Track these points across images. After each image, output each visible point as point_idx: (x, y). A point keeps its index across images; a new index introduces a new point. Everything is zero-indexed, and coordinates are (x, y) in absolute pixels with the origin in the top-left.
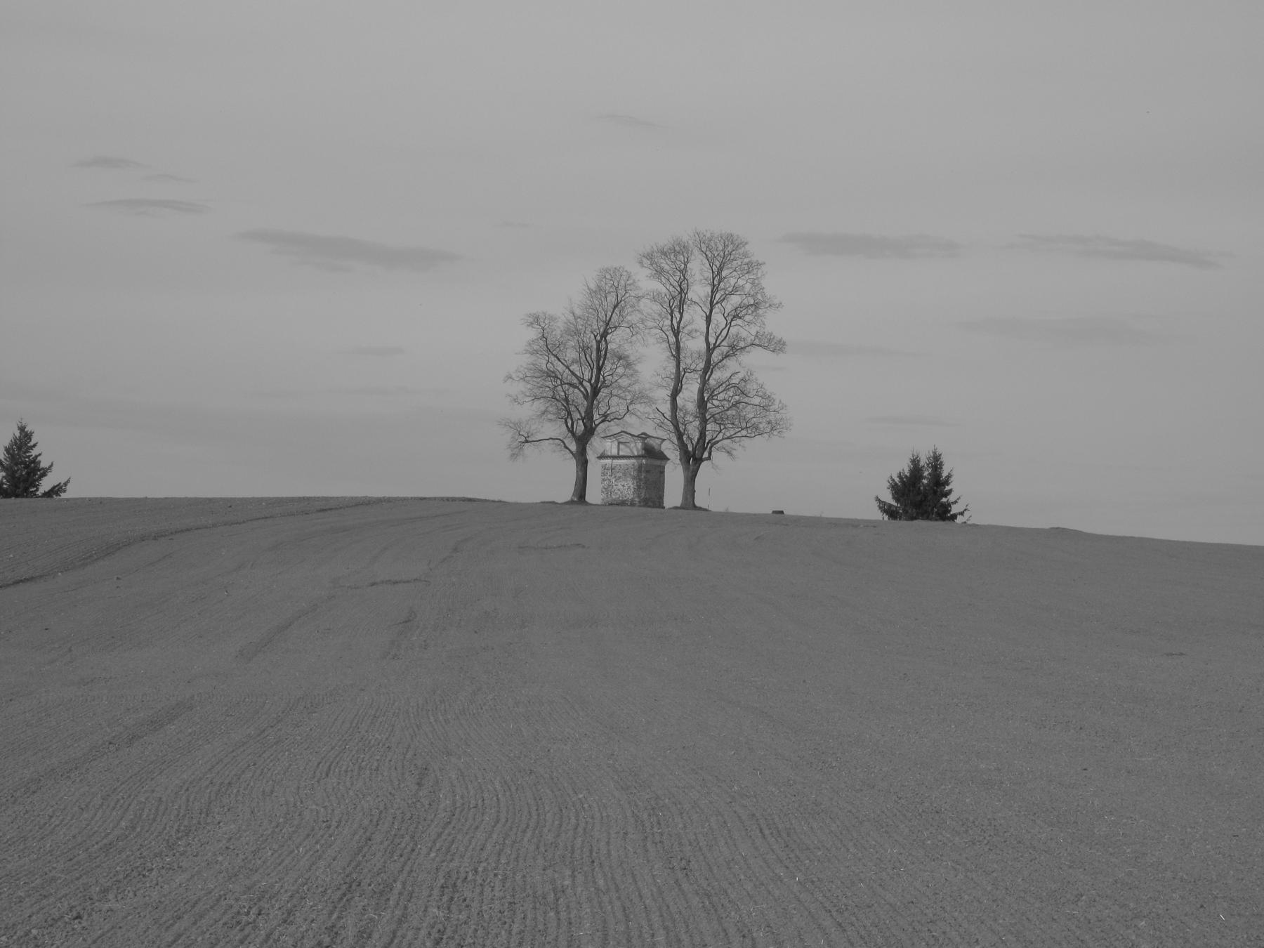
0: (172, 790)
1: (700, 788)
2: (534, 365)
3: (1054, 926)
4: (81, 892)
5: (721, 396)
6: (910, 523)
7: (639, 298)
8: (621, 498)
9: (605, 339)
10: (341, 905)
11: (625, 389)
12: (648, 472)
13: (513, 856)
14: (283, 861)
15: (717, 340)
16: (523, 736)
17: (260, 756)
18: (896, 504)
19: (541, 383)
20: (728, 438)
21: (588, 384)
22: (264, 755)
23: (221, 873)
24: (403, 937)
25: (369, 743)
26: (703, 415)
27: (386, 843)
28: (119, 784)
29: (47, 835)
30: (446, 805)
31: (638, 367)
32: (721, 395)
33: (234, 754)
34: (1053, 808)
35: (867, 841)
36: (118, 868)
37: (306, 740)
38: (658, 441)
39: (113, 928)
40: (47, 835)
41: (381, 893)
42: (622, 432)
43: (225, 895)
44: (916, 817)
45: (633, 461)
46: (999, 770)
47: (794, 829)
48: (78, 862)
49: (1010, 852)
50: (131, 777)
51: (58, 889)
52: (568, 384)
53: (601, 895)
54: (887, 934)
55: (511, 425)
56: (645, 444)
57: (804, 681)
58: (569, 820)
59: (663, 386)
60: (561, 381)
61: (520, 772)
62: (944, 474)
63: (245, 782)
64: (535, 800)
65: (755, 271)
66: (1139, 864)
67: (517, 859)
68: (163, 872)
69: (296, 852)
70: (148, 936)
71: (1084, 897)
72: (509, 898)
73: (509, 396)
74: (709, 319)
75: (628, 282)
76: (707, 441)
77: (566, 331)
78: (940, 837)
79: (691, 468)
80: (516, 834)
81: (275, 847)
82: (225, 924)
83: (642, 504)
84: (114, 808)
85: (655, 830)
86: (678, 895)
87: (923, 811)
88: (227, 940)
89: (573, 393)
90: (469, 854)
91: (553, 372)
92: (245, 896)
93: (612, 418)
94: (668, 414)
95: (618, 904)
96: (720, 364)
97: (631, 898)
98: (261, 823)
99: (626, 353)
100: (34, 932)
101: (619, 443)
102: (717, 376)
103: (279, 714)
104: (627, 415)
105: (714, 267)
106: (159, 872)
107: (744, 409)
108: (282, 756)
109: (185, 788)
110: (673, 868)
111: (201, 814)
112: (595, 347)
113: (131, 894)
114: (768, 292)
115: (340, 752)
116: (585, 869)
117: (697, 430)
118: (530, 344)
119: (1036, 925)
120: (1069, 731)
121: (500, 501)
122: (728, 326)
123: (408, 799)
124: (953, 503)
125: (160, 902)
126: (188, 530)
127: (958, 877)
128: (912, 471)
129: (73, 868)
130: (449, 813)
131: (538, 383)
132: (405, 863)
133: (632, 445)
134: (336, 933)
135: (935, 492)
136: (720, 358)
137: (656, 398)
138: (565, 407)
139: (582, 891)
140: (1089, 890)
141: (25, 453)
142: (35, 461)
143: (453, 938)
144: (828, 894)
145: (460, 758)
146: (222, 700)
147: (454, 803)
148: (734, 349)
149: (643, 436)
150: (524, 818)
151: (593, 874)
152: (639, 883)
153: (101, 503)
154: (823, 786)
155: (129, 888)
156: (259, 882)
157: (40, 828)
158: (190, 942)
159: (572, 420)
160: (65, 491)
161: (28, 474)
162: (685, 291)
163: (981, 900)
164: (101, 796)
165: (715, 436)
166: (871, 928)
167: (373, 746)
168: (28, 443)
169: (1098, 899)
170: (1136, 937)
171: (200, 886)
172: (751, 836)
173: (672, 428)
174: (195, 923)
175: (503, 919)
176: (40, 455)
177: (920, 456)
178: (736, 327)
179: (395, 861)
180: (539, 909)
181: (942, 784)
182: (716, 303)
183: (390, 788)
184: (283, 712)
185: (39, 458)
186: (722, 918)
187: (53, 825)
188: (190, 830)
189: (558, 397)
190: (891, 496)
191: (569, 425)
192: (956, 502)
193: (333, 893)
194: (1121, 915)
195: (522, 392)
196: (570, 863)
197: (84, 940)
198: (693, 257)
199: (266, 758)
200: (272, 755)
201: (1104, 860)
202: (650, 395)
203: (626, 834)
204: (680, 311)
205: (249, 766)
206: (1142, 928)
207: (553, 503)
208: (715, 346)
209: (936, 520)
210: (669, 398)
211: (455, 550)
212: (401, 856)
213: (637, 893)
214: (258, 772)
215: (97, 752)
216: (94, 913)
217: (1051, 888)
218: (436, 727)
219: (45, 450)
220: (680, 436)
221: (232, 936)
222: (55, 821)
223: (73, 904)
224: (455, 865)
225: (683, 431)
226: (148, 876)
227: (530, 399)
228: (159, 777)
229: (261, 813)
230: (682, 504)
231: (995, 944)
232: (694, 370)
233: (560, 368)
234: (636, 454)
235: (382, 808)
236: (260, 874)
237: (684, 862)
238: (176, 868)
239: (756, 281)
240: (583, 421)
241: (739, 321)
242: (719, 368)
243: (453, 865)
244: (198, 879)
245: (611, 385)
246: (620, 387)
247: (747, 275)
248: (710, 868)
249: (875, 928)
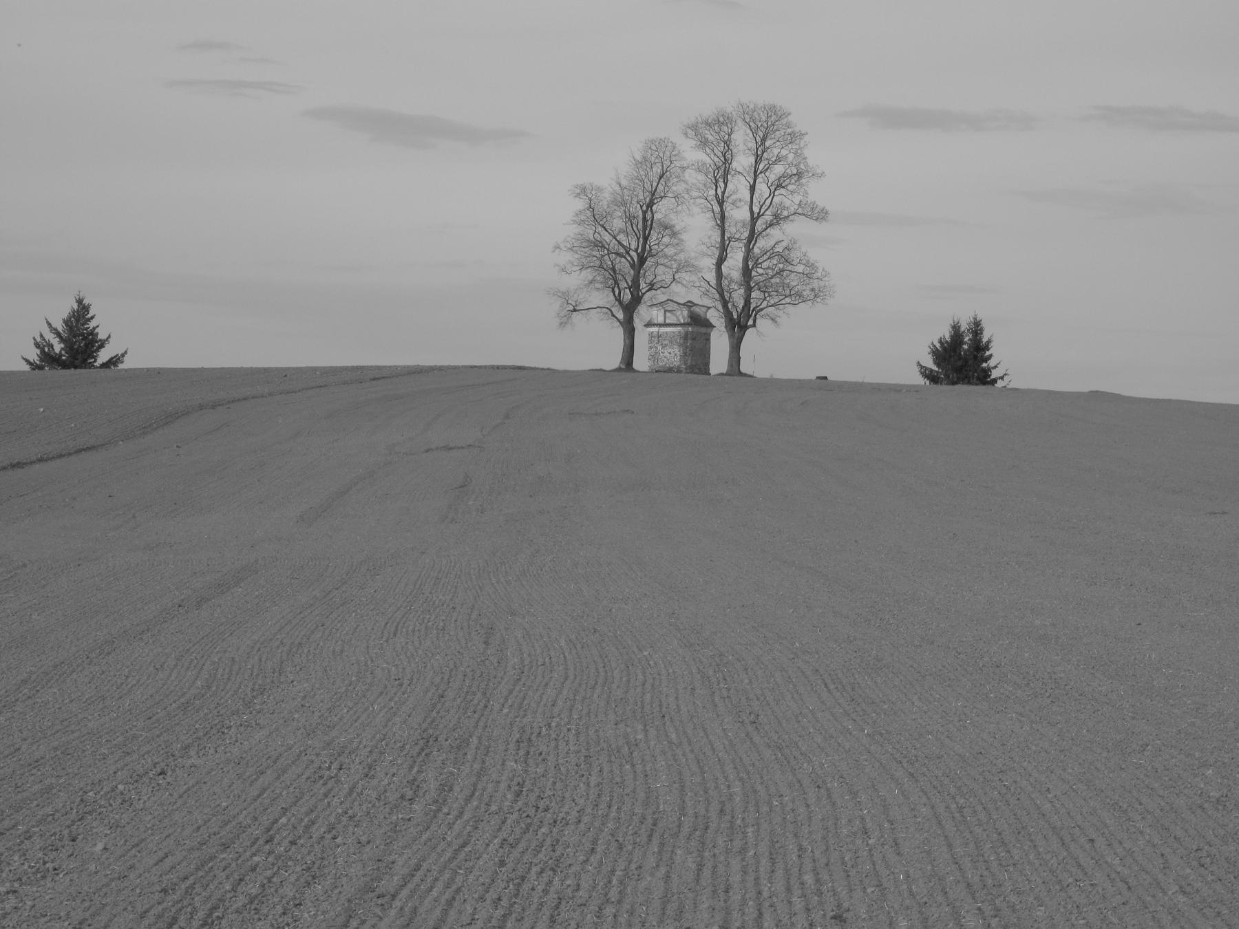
0: (244, 651)
1: (762, 645)
2: (582, 235)
3: (1124, 775)
4: (163, 749)
5: (765, 265)
6: (950, 387)
7: (684, 169)
9: (651, 209)
10: (421, 759)
11: (671, 258)
12: (694, 339)
13: (584, 712)
14: (358, 718)
15: (760, 209)
16: (584, 596)
17: (327, 617)
18: (937, 369)
19: (588, 253)
20: (772, 306)
21: (635, 254)
22: (331, 616)
23: (298, 730)
24: (484, 789)
25: (434, 604)
26: (748, 283)
27: (459, 700)
28: (191, 645)
29: (126, 694)
30: (514, 663)
31: (684, 237)
32: (765, 263)
33: (302, 615)
34: (1110, 661)
35: (931, 695)
36: (197, 726)
37: (371, 601)
38: (704, 309)
39: (197, 783)
40: (126, 694)
41: (459, 747)
42: (668, 300)
43: (305, 751)
44: (977, 671)
45: (679, 328)
46: (1054, 625)
47: (858, 683)
48: (158, 720)
49: (1073, 704)
50: (203, 638)
51: (140, 746)
52: (614, 253)
53: (675, 748)
54: (959, 784)
55: (559, 294)
56: (691, 311)
57: (856, 541)
58: (637, 676)
59: (708, 255)
60: (608, 250)
61: (584, 631)
62: (985, 340)
63: (315, 642)
64: (602, 657)
65: (798, 142)
66: (1201, 715)
67: (588, 714)
68: (242, 729)
69: (371, 709)
70: (233, 790)
71: (1149, 747)
72: (584, 752)
73: (557, 265)
74: (752, 189)
75: (674, 153)
76: (751, 309)
77: (613, 201)
78: (1002, 691)
79: (736, 335)
80: (585, 690)
81: (350, 704)
82: (308, 778)
83: (688, 371)
84: (188, 668)
85: (722, 685)
86: (750, 748)
87: (984, 666)
88: (311, 794)
89: (620, 262)
90: (540, 710)
91: (600, 242)
92: (326, 752)
93: (659, 286)
94: (713, 282)
95: (691, 756)
96: (764, 233)
97: (703, 751)
98: (334, 681)
99: (671, 223)
100: (121, 787)
101: (665, 311)
102: (761, 244)
103: (344, 577)
104: (673, 284)
105: (758, 137)
106: (238, 729)
107: (787, 276)
108: (349, 617)
109: (256, 648)
110: (743, 722)
111: (273, 673)
112: (641, 216)
113: (212, 751)
114: (811, 162)
115: (406, 613)
116: (656, 723)
117: (742, 298)
118: (577, 215)
119: (1104, 774)
120: (1120, 587)
121: (548, 369)
122: (772, 195)
123: (477, 657)
125: (241, 757)
126: (245, 399)
127: (1024, 729)
128: (952, 337)
129: (153, 726)
130: (519, 671)
131: (586, 253)
132: (479, 719)
133: (679, 313)
134: (418, 786)
135: (975, 357)
136: (764, 227)
137: (701, 267)
138: (612, 276)
139: (655, 744)
140: (1153, 740)
141: (83, 325)
142: (92, 333)
143: (532, 790)
144: (897, 746)
145: (524, 617)
146: (286, 563)
147: (522, 660)
148: (777, 219)
149: (689, 304)
150: (592, 675)
151: (665, 728)
152: (711, 737)
153: (159, 373)
154: (883, 642)
155: (210, 745)
156: (337, 737)
157: (117, 688)
158: (275, 796)
159: (619, 289)
160: (122, 362)
161: (86, 345)
162: (729, 162)
163: (1048, 751)
164: (175, 657)
165: (759, 304)
166: (943, 779)
167: (438, 607)
168: (86, 315)
169: (1163, 748)
170: (1205, 785)
171: (279, 743)
172: (816, 691)
173: (717, 296)
174: (278, 778)
175: (579, 772)
176: (98, 326)
177: (960, 322)
178: (781, 196)
179: (469, 717)
180: (614, 762)
181: (999, 640)
182: (761, 173)
183: (458, 648)
184: (347, 575)
185: (96, 331)
186: (795, 770)
187: (130, 685)
188: (264, 689)
189: (605, 267)
190: (932, 361)
191: (617, 293)
192: (996, 367)
193: (411, 748)
194: (1188, 763)
195: (569, 261)
196: (641, 718)
197: (170, 795)
198: (737, 128)
199: (334, 618)
200: (339, 616)
201: (1166, 712)
202: (696, 263)
203: (693, 689)
204: (724, 182)
205: (317, 626)
206: (1209, 776)
207: (601, 370)
208: (759, 216)
209: (976, 384)
210: (714, 267)
211: (507, 417)
212: (475, 712)
213: (710, 747)
214: (327, 632)
215: (167, 614)
216: (177, 769)
217: (1116, 738)
218: (498, 588)
219: (102, 322)
220: (725, 304)
221: (316, 790)
222: (131, 681)
223: (156, 761)
224: (528, 720)
225: (728, 299)
226: (227, 733)
227: (578, 268)
228: (229, 638)
229: (333, 671)
230: (727, 371)
231: (1066, 793)
232: (738, 239)
233: (607, 238)
234: (682, 321)
235: (452, 666)
236: (338, 730)
237: (752, 716)
238: (254, 724)
239: (799, 151)
240: (630, 290)
241: (782, 191)
242: (763, 237)
243: (525, 721)
244: (277, 736)
245: (657, 254)
246: (666, 256)
247: (790, 145)
248: (779, 722)
249: (946, 778)
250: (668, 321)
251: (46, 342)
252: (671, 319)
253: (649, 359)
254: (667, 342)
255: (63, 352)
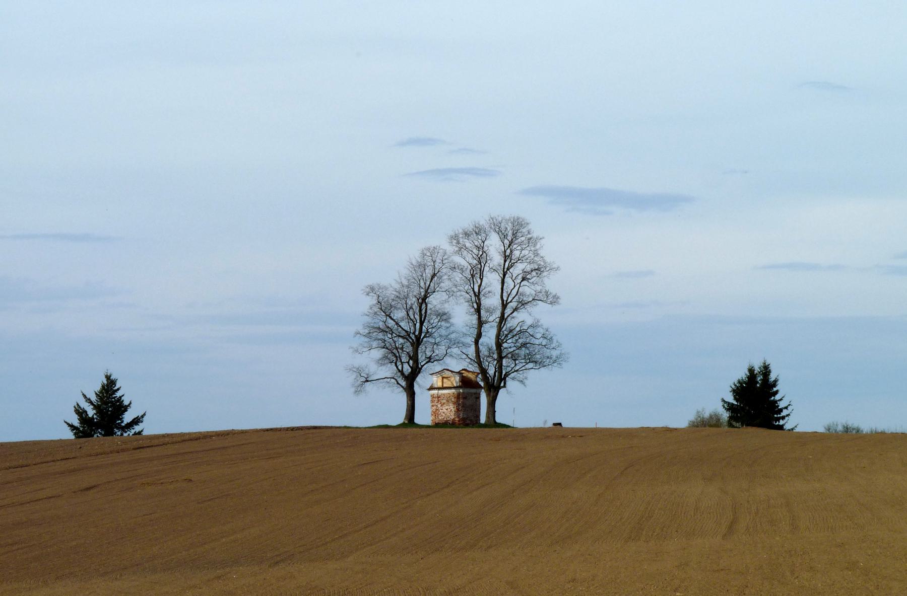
8: (445, 419)
12: (465, 398)
18: (736, 403)
45: (453, 391)
56: (463, 377)
76: (504, 374)
101: (443, 378)
124: (779, 400)
142: (120, 400)
160: (142, 422)
168: (114, 387)
176: (123, 396)
185: (123, 398)
190: (733, 398)
191: (400, 368)
192: (781, 400)
204: (480, 278)
219: (126, 392)
230: (486, 421)
234: (455, 385)
250: (445, 386)
251: (82, 409)
252: (447, 384)
253: (432, 415)
254: (444, 401)
255: (95, 416)
